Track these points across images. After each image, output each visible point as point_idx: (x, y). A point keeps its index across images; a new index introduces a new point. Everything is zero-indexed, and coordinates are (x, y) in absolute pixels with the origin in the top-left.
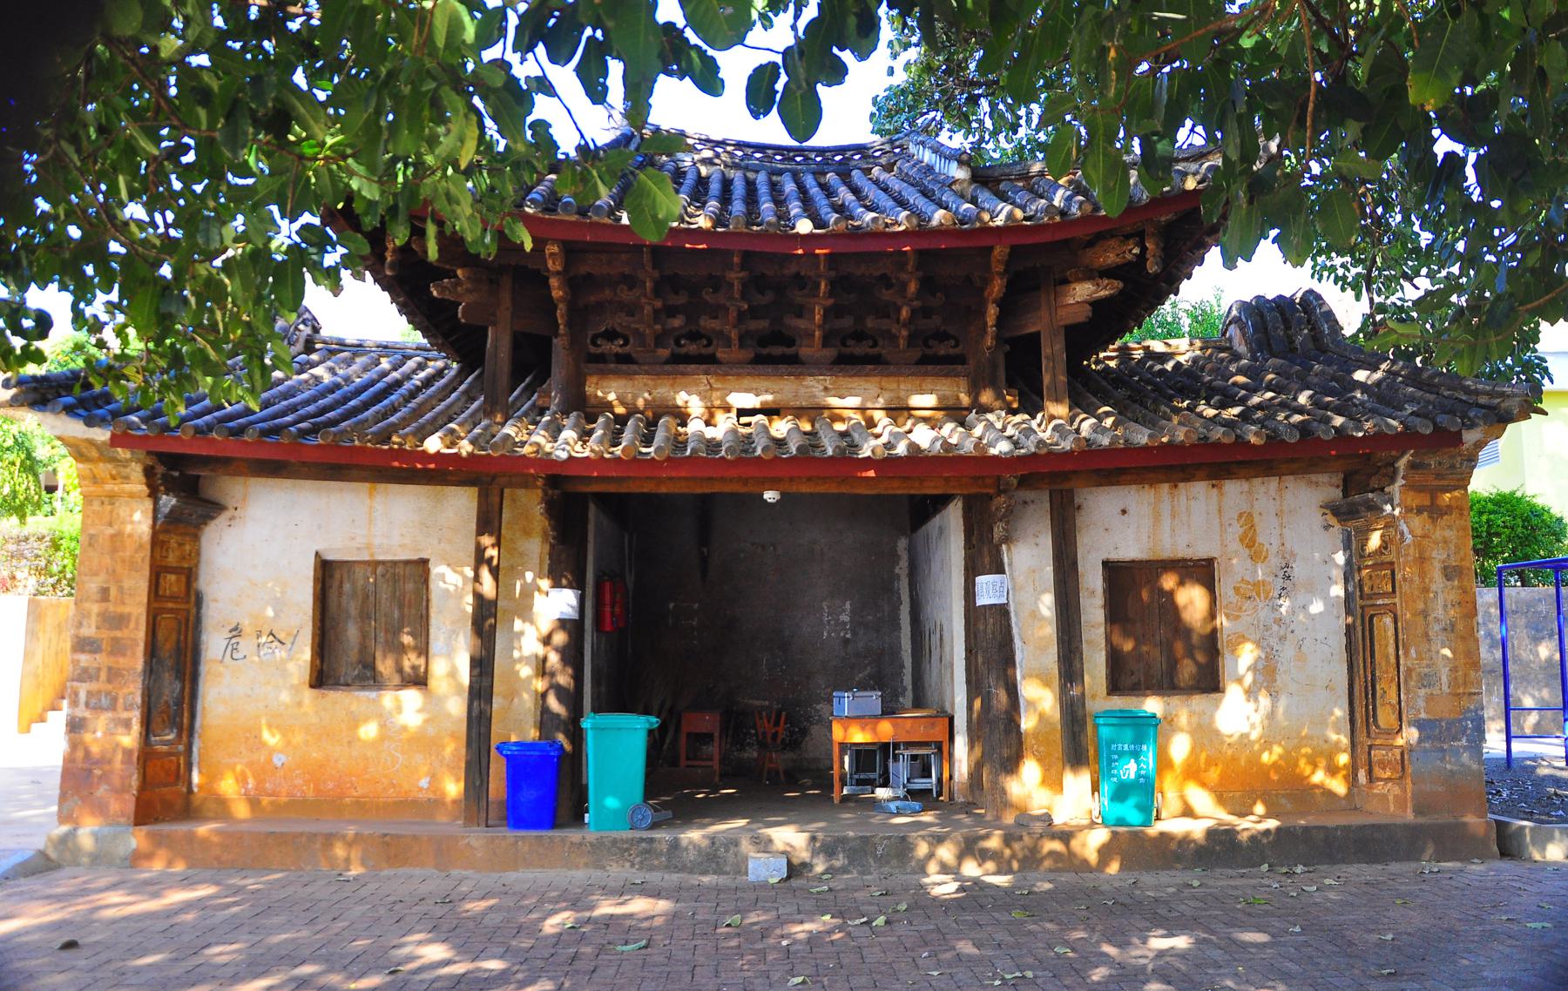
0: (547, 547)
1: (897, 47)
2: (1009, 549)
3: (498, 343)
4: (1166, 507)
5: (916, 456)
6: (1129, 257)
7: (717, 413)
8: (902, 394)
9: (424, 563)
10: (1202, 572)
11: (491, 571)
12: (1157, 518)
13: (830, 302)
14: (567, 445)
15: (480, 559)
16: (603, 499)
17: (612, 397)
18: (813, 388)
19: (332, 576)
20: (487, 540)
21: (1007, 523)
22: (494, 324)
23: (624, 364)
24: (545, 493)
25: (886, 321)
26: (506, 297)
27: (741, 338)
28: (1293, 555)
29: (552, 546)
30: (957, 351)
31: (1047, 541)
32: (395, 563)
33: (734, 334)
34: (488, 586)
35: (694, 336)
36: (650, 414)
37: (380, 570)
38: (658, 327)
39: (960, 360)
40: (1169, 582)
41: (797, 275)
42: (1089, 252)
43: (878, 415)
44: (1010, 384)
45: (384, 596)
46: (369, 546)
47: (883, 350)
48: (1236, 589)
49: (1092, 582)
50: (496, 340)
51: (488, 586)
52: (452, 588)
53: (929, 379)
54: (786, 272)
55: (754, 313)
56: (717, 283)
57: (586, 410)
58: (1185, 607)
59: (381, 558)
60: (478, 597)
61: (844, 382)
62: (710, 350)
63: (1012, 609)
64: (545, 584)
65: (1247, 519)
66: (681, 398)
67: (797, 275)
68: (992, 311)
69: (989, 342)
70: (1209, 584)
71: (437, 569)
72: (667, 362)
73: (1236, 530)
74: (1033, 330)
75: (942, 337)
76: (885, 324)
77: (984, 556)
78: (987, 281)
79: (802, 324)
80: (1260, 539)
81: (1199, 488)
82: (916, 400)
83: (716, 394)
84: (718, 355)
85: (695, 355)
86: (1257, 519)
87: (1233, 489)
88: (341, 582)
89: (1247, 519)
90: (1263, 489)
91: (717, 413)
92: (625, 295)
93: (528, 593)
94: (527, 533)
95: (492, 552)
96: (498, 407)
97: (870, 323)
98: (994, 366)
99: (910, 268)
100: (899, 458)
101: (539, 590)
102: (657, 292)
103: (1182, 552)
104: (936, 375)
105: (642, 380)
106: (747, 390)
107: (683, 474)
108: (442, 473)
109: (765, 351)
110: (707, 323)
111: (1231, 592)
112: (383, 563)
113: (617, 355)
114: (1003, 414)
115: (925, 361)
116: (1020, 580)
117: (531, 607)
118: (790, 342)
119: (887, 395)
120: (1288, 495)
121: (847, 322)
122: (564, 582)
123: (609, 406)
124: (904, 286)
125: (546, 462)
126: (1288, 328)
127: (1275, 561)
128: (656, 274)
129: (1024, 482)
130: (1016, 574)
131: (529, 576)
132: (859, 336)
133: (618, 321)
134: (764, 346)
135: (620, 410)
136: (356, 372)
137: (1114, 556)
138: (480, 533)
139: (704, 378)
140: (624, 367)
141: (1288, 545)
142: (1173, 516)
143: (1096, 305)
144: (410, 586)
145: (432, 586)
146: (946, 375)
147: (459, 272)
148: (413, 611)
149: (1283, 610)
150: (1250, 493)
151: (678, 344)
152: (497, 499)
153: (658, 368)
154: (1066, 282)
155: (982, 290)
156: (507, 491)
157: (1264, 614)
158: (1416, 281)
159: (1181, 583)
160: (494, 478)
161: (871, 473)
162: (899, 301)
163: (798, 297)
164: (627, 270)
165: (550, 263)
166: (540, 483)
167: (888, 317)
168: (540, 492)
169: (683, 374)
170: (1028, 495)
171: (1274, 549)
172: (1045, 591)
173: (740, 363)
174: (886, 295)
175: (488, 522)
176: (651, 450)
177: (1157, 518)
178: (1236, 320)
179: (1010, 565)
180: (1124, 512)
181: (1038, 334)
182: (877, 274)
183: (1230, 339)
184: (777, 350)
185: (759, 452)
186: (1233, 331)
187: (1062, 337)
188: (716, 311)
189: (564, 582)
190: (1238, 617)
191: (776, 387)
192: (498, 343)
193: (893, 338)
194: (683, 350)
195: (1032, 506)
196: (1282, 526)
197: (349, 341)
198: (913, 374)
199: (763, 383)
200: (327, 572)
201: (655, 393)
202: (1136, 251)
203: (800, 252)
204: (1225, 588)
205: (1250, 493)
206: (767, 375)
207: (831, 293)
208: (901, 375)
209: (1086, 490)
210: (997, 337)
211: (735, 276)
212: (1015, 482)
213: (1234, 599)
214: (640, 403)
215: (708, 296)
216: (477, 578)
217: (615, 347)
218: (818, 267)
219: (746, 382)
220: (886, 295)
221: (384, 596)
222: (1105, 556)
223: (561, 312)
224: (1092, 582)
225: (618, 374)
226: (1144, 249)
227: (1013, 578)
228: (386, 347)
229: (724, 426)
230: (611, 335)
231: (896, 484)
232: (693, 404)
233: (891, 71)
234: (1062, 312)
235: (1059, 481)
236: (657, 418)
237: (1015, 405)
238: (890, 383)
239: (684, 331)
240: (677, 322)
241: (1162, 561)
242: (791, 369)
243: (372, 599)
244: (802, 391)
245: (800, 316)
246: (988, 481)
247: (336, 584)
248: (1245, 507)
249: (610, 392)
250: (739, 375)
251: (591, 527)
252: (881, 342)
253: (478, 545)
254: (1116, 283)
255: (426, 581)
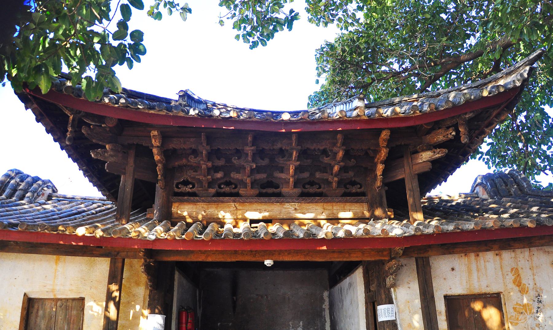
0: (148, 292)
1: (320, 70)
2: (395, 290)
3: (126, 183)
4: (474, 266)
5: (349, 239)
6: (450, 136)
7: (238, 219)
8: (335, 211)
9: (82, 299)
10: (495, 300)
11: (115, 304)
12: (470, 272)
13: (298, 163)
14: (157, 232)
15: (109, 297)
16: (183, 267)
17: (185, 214)
18: (289, 209)
19: (33, 307)
20: (114, 287)
21: (396, 276)
22: (124, 174)
23: (191, 197)
24: (146, 261)
25: (325, 174)
26: (131, 161)
27: (252, 183)
28: (541, 290)
29: (151, 291)
30: (362, 190)
31: (415, 287)
32: (67, 300)
33: (248, 180)
34: (113, 313)
35: (228, 184)
36: (205, 223)
37: (59, 303)
38: (209, 177)
39: (363, 194)
40: (477, 306)
41: (281, 149)
42: (428, 137)
43: (322, 222)
44: (389, 206)
45: (60, 318)
46: (53, 291)
47: (324, 189)
48: (514, 309)
49: (441, 306)
50: (125, 181)
51: (113, 313)
52: (96, 314)
53: (348, 204)
54: (275, 147)
55: (258, 170)
56: (239, 153)
57: (169, 218)
58: (488, 320)
59: (59, 297)
60: (107, 318)
61: (305, 206)
62: (236, 190)
63: (398, 322)
64: (146, 312)
65: (516, 271)
66: (221, 214)
67: (281, 149)
68: (380, 167)
69: (379, 183)
70: (499, 306)
71: (89, 304)
72: (214, 196)
73: (510, 277)
74: (401, 177)
75: (353, 183)
76: (325, 176)
77: (377, 295)
78: (377, 152)
79: (283, 176)
80: (524, 282)
81: (490, 256)
82: (342, 215)
83: (239, 212)
84: (240, 192)
85: (227, 191)
86: (521, 271)
87: (507, 255)
88: (38, 310)
89: (516, 271)
90: (521, 256)
91: (238, 219)
92: (193, 160)
93: (136, 317)
94: (137, 284)
95: (116, 294)
96: (121, 215)
97: (318, 175)
98: (381, 197)
99: (339, 145)
100: (340, 239)
101: (143, 315)
102: (209, 157)
103: (484, 290)
104: (351, 202)
105: (201, 205)
106: (255, 210)
107: (220, 249)
108: (88, 249)
109: (264, 191)
110: (235, 176)
111: (512, 310)
112: (61, 299)
113: (189, 192)
114: (387, 220)
115: (345, 195)
116: (402, 307)
117: (138, 324)
118: (277, 187)
119: (327, 212)
120: (535, 258)
121: (306, 175)
122: (157, 311)
123: (184, 218)
124: (335, 154)
125: (145, 241)
126: (507, 185)
127: (532, 293)
128: (208, 148)
129: (407, 253)
130: (399, 304)
131: (138, 307)
132: (312, 184)
133: (189, 175)
134: (264, 188)
135: (189, 220)
136: (66, 207)
137: (450, 293)
138: (110, 283)
139: (233, 204)
140: (192, 198)
141: (538, 285)
142: (478, 271)
143: (434, 162)
144: (74, 312)
145: (85, 312)
146: (357, 202)
147: (107, 146)
148: (75, 326)
149: (540, 319)
150: (515, 258)
151: (220, 187)
152: (120, 265)
153: (209, 199)
154: (417, 152)
155: (373, 158)
156: (126, 260)
157: (530, 321)
158: (545, 171)
159: (485, 307)
160: (118, 253)
161: (325, 248)
162: (333, 163)
163: (280, 161)
164: (193, 147)
165: (153, 141)
166: (141, 254)
167: (327, 173)
168: (143, 260)
169: (223, 202)
170: (403, 261)
171: (531, 286)
172: (415, 313)
173: (251, 196)
174: (326, 160)
175: (115, 276)
176: (202, 236)
177: (470, 272)
178: (480, 184)
179: (396, 299)
180: (453, 269)
181: (403, 180)
182: (322, 148)
183: (477, 193)
184: (271, 190)
185: (262, 235)
186: (479, 189)
187: (416, 180)
188: (239, 169)
189: (157, 311)
190: (517, 324)
191: (270, 209)
192: (126, 183)
193: (329, 183)
194: (222, 191)
195: (405, 268)
196: (534, 275)
197: (68, 196)
198: (340, 202)
199: (263, 207)
200: (30, 305)
201: (208, 211)
202: (454, 133)
203: (284, 131)
204: (508, 308)
205: (515, 258)
206: (266, 202)
207: (299, 158)
208: (334, 202)
209: (436, 257)
210: (383, 181)
211: (249, 150)
212: (401, 252)
213: (514, 314)
214: (200, 217)
215: (235, 161)
216: (107, 308)
217: (188, 189)
218: (291, 144)
219: (255, 206)
220: (326, 160)
221: (60, 318)
222: (445, 293)
223: (159, 167)
224: (441, 306)
225: (189, 202)
226: (458, 132)
227: (398, 306)
228: (85, 199)
229: (242, 227)
230: (186, 183)
231: (336, 255)
232: (226, 215)
233: (317, 82)
234: (416, 167)
235: (420, 252)
236: (208, 224)
237: (393, 217)
238: (328, 206)
239: (222, 181)
240: (219, 175)
241: (474, 295)
242: (277, 199)
243: (53, 319)
244: (284, 210)
245: (282, 172)
246: (385, 253)
247: (35, 311)
248: (514, 265)
249: (184, 211)
250: (251, 202)
251: (176, 283)
252: (323, 186)
253: (108, 289)
254: (444, 150)
255: (83, 310)
